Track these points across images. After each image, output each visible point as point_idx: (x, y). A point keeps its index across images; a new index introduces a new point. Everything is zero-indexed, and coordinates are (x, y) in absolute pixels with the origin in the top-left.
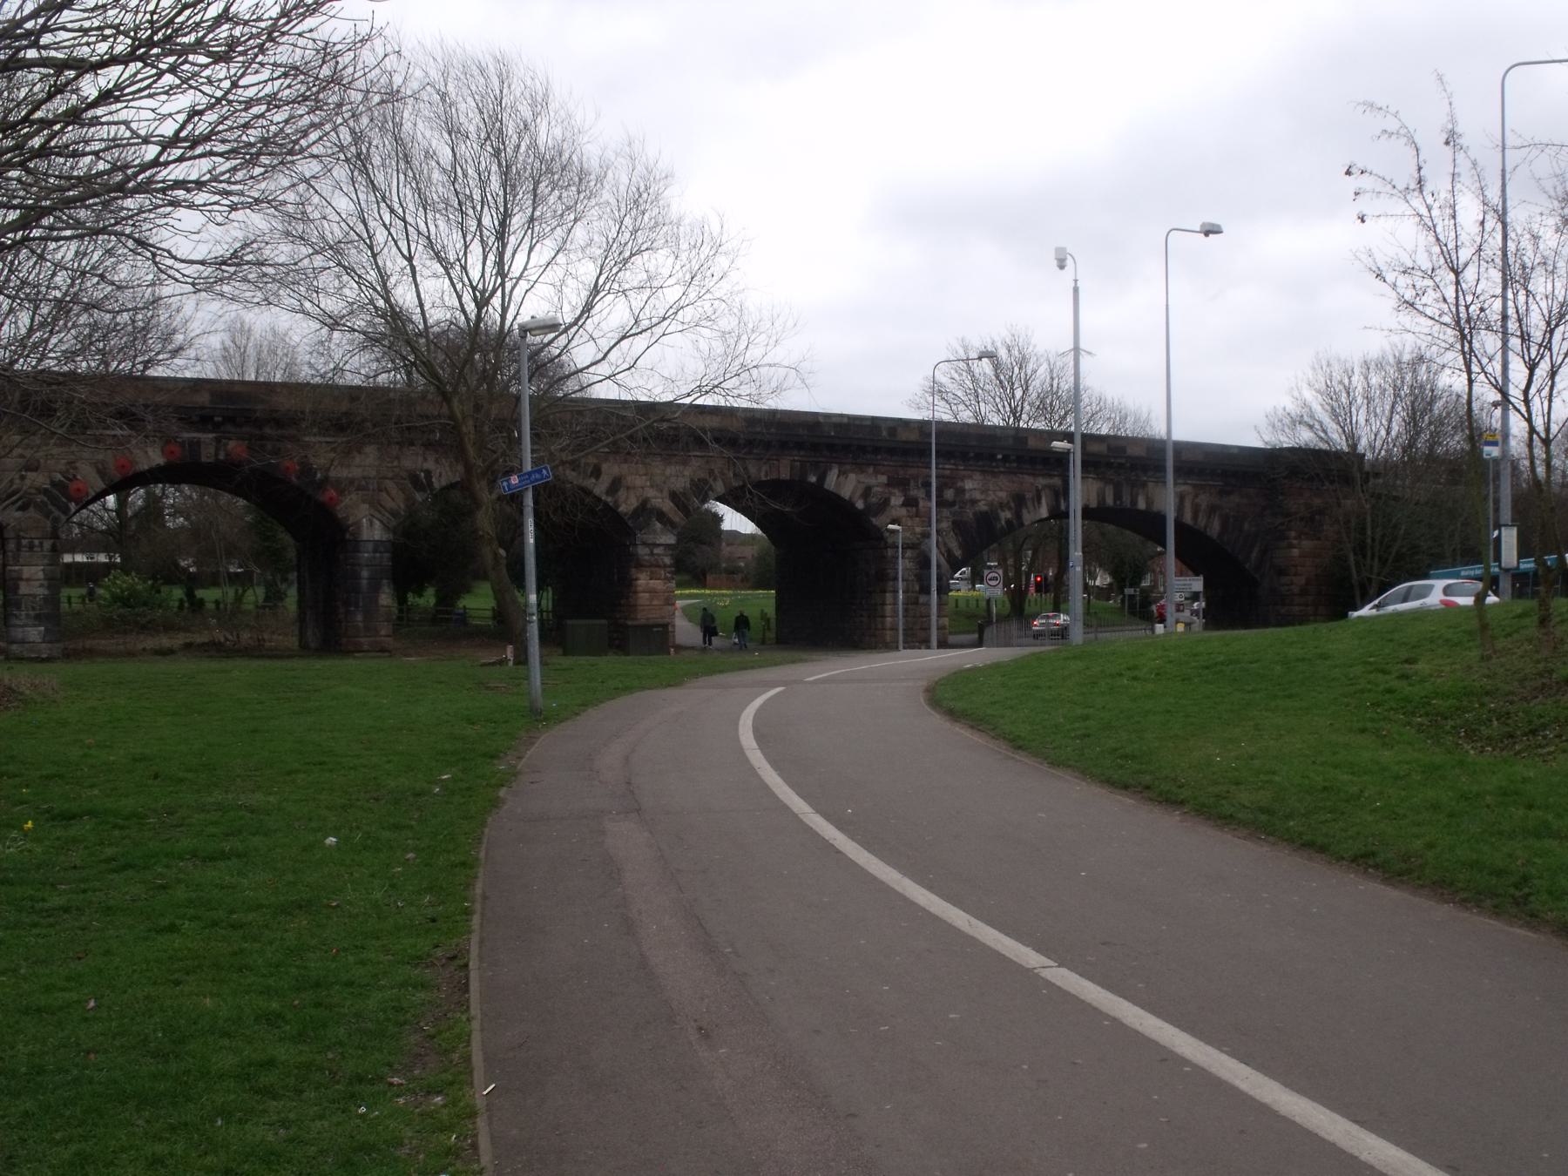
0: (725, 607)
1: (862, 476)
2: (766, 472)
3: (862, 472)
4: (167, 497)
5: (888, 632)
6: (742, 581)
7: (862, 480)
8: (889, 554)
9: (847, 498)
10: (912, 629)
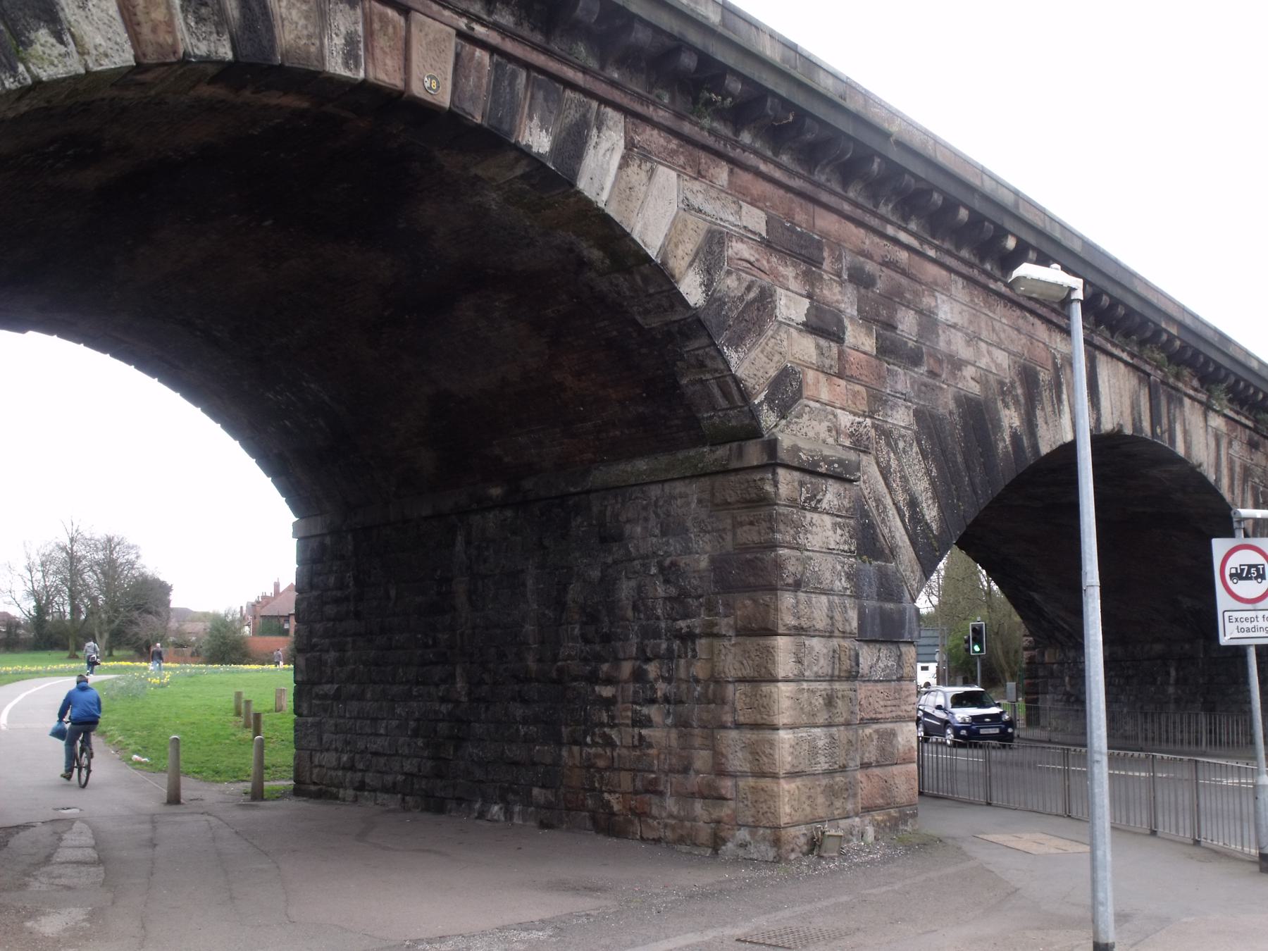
0: (162, 686)
1: (697, 186)
2: (351, 41)
3: (699, 175)
4: (887, 787)
5: (786, 786)
6: (192, 655)
7: (698, 201)
8: (784, 490)
9: (652, 253)
10: (843, 768)
